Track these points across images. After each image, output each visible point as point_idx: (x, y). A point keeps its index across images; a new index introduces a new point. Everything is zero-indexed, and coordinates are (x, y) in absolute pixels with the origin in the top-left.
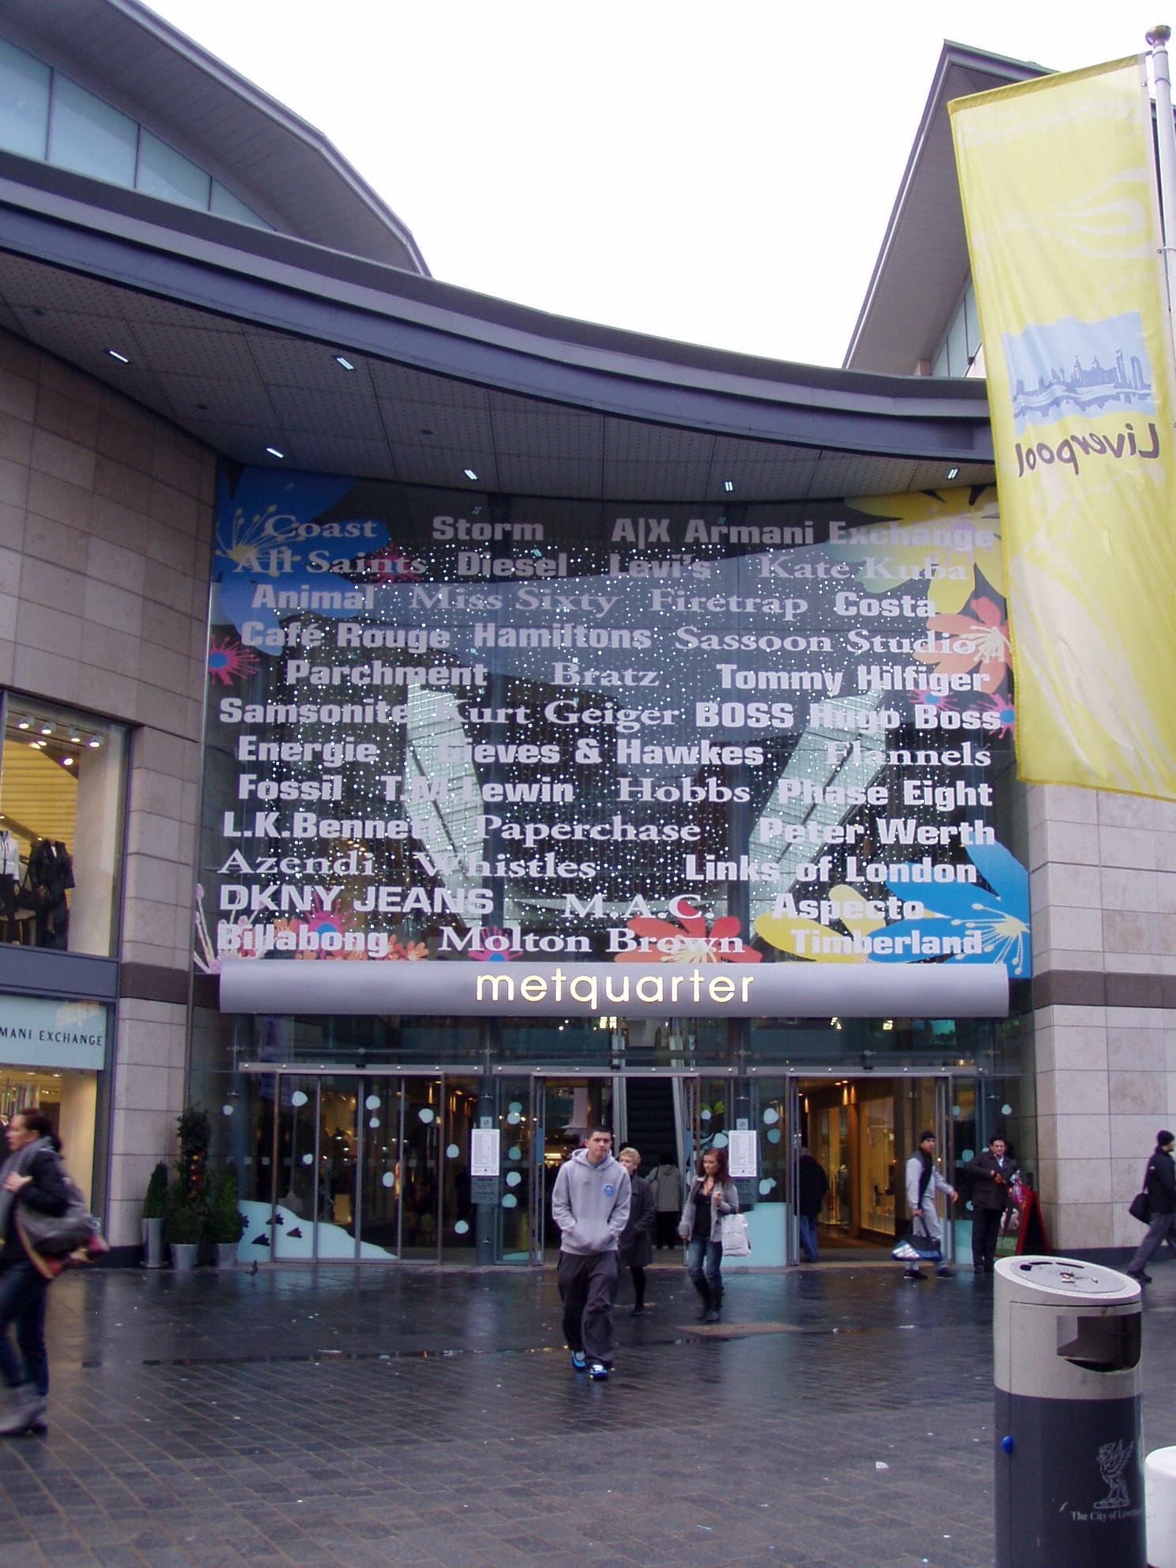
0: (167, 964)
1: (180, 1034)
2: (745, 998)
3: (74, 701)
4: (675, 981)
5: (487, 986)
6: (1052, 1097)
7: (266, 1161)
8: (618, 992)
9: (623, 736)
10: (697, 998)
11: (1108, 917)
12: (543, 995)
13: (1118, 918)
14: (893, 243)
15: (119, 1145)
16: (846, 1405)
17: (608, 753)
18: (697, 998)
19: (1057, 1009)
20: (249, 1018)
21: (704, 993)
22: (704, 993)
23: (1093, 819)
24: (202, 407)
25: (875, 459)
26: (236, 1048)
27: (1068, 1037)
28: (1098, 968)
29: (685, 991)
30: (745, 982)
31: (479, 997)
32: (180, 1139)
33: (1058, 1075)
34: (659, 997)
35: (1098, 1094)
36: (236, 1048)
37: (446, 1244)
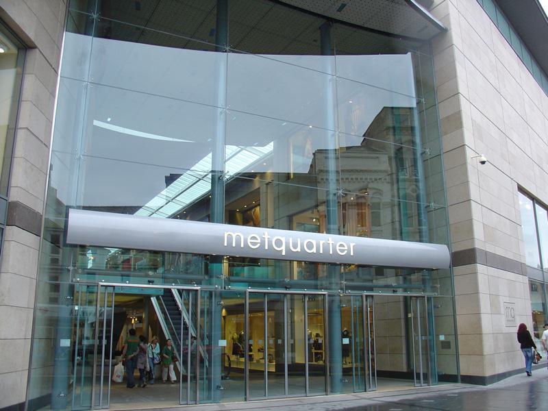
2: (352, 254)
5: (230, 238)
7: (423, 338)
8: (295, 247)
9: (230, 365)
10: (331, 253)
12: (259, 245)
15: (404, 357)
16: (429, 313)
17: (163, 363)
18: (331, 253)
21: (334, 250)
22: (334, 250)
29: (326, 247)
30: (352, 245)
31: (226, 244)
32: (239, 316)
34: (314, 250)
37: (64, 246)
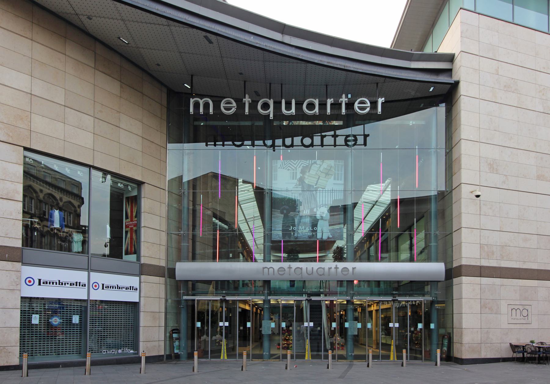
0: (158, 264)
1: (163, 287)
3: (118, 172)
4: (329, 101)
6: (461, 306)
11: (481, 246)
12: (368, 109)
13: (486, 247)
14: (409, 7)
19: (464, 278)
20: (186, 282)
23: (478, 213)
24: (158, 65)
25: (405, 82)
26: (182, 292)
27: (467, 288)
28: (478, 264)
33: (463, 300)
35: (477, 307)
36: (182, 292)
